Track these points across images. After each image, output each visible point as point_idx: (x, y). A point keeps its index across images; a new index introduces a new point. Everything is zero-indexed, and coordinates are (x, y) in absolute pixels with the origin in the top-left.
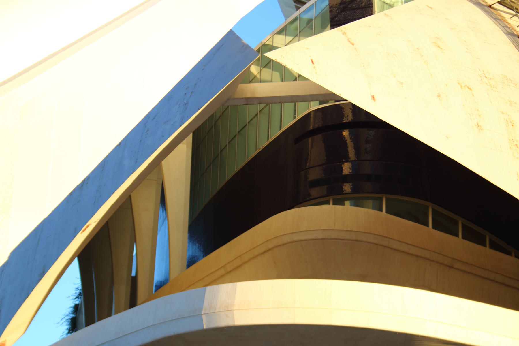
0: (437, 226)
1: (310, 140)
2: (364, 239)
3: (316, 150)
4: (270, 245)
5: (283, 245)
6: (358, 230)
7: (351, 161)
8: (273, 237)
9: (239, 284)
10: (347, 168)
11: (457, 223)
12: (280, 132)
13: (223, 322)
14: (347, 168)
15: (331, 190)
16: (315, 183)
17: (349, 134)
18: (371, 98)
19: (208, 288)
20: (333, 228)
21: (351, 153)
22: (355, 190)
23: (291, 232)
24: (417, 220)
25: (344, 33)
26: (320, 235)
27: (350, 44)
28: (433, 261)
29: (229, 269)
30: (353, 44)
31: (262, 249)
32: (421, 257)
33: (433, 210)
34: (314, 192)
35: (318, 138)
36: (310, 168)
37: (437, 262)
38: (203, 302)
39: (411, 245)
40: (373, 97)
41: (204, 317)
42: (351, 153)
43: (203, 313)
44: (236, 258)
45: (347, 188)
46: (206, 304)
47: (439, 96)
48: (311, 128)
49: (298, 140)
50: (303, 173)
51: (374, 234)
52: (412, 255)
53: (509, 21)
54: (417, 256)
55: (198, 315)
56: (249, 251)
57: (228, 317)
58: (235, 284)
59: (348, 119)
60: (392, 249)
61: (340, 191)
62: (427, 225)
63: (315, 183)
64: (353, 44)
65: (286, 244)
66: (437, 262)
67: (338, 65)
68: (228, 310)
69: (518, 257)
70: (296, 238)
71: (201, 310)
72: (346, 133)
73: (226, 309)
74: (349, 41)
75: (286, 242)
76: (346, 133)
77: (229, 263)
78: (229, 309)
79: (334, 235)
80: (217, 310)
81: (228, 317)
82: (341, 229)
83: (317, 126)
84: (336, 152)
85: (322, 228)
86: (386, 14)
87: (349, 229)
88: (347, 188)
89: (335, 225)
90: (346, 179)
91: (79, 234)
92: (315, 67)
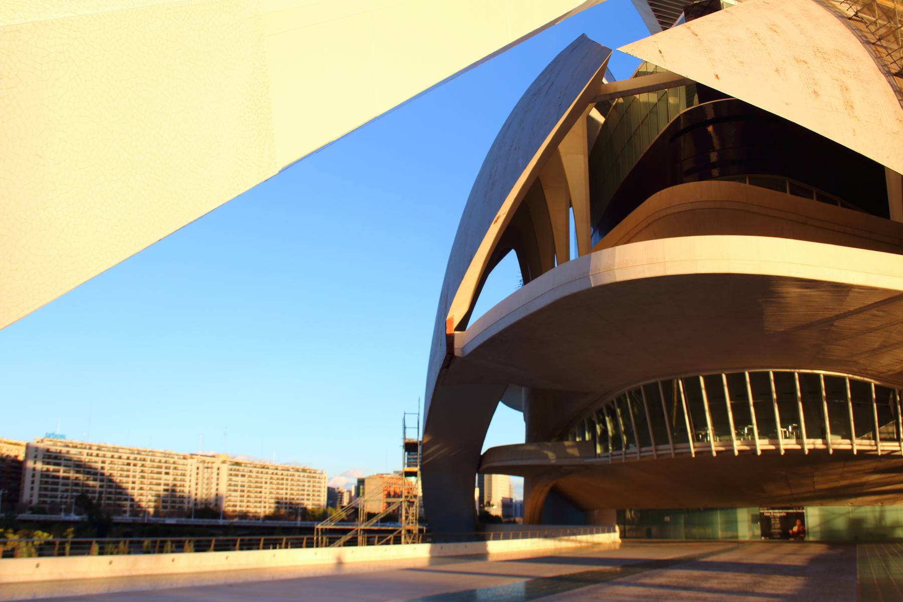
10: (714, 157)
12: (657, 136)
13: (607, 280)
14: (714, 157)
15: (702, 173)
21: (716, 145)
25: (689, 28)
27: (692, 35)
33: (790, 183)
40: (717, 76)
42: (716, 145)
45: (715, 172)
46: (592, 267)
47: (777, 70)
48: (682, 128)
53: (840, 7)
67: (686, 52)
68: (610, 270)
71: (588, 272)
72: (710, 129)
91: (492, 225)
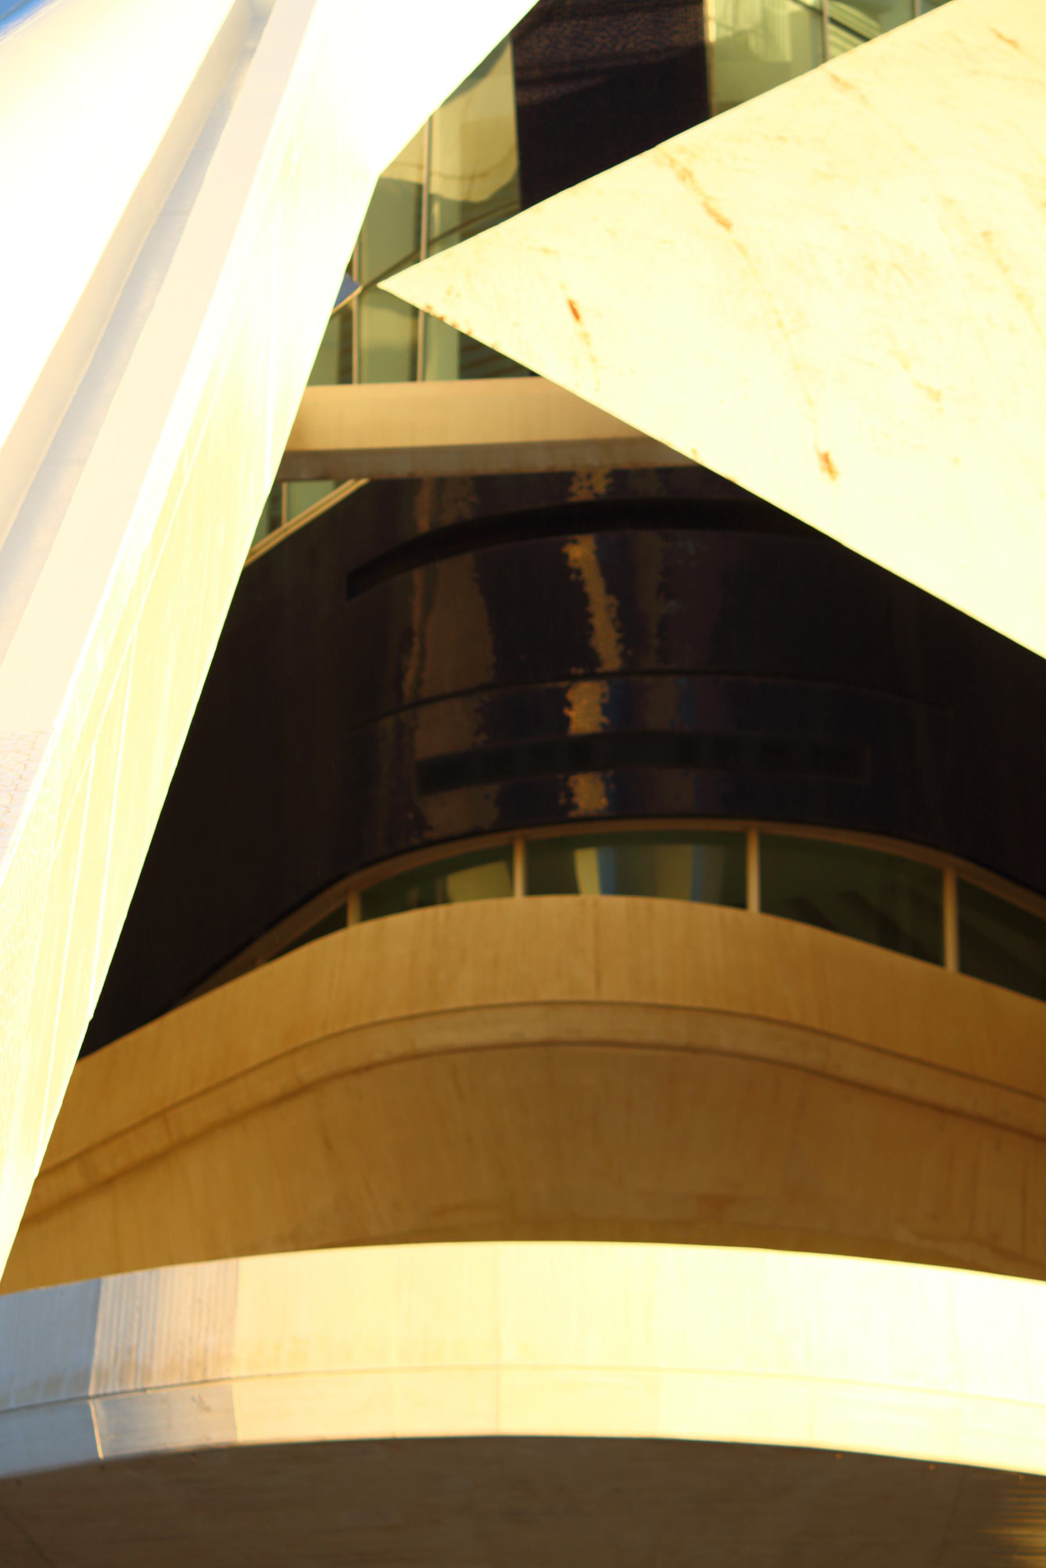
0: (979, 961)
1: (418, 576)
2: (725, 1042)
3: (447, 625)
4: (308, 1072)
5: (368, 1068)
6: (699, 1004)
7: (608, 676)
8: (318, 1035)
9: (250, 1265)
10: (585, 710)
11: (936, 879)
13: (186, 1430)
14: (585, 710)
16: (444, 774)
17: (599, 553)
18: (817, 463)
19: (111, 1283)
20: (591, 997)
21: (606, 642)
22: (625, 804)
23: (404, 1012)
24: (888, 934)
25: (686, 175)
26: (534, 1027)
28: (1007, 1128)
29: (106, 1169)
30: (726, 225)
31: (267, 1087)
32: (957, 1113)
34: (446, 811)
35: (458, 574)
36: (420, 702)
37: (1026, 1134)
38: (91, 1343)
39: (920, 1062)
40: (826, 458)
41: (96, 1409)
42: (606, 642)
43: (92, 1392)
44: (146, 1121)
45: (588, 792)
46: (103, 1352)
48: (424, 525)
49: (361, 577)
50: (388, 723)
51: (767, 1020)
52: (920, 1104)
54: (940, 1109)
55: (67, 1394)
56: (206, 1091)
57: (207, 1409)
58: (230, 1263)
59: (591, 488)
60: (841, 1081)
61: (556, 809)
62: (936, 957)
63: (444, 774)
64: (726, 225)
65: (381, 1064)
66: (1026, 1134)
69: (1028, 958)
70: (428, 1037)
71: (83, 1378)
73: (198, 1377)
74: (711, 212)
75: (380, 1056)
76: (581, 551)
77: (105, 1142)
78: (210, 1376)
79: (596, 1026)
80: (155, 1382)
81: (207, 1409)
82: (628, 998)
83: (449, 518)
84: (538, 639)
85: (545, 997)
86: (835, 78)
87: (661, 1000)
88: (588, 792)
89: (598, 982)
90: (583, 753)
92: (585, 336)
